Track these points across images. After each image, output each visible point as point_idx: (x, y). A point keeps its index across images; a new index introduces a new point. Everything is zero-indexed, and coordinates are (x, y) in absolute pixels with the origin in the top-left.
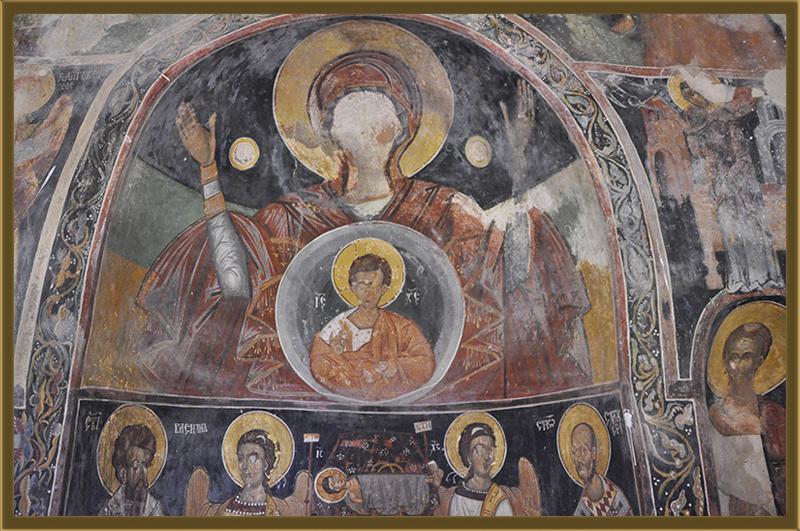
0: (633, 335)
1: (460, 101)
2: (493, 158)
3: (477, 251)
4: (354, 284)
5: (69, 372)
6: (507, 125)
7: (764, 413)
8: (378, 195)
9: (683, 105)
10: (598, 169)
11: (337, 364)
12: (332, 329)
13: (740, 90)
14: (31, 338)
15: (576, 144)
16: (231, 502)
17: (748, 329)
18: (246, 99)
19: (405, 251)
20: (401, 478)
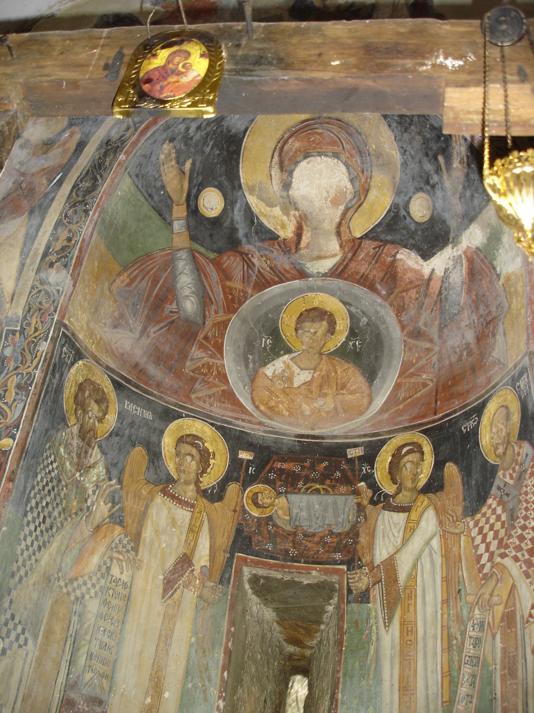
1: (405, 162)
2: (433, 211)
4: (300, 332)
5: (57, 307)
6: (445, 177)
11: (277, 397)
12: (276, 366)
16: (164, 488)
18: (218, 152)
19: (350, 305)
20: (329, 499)
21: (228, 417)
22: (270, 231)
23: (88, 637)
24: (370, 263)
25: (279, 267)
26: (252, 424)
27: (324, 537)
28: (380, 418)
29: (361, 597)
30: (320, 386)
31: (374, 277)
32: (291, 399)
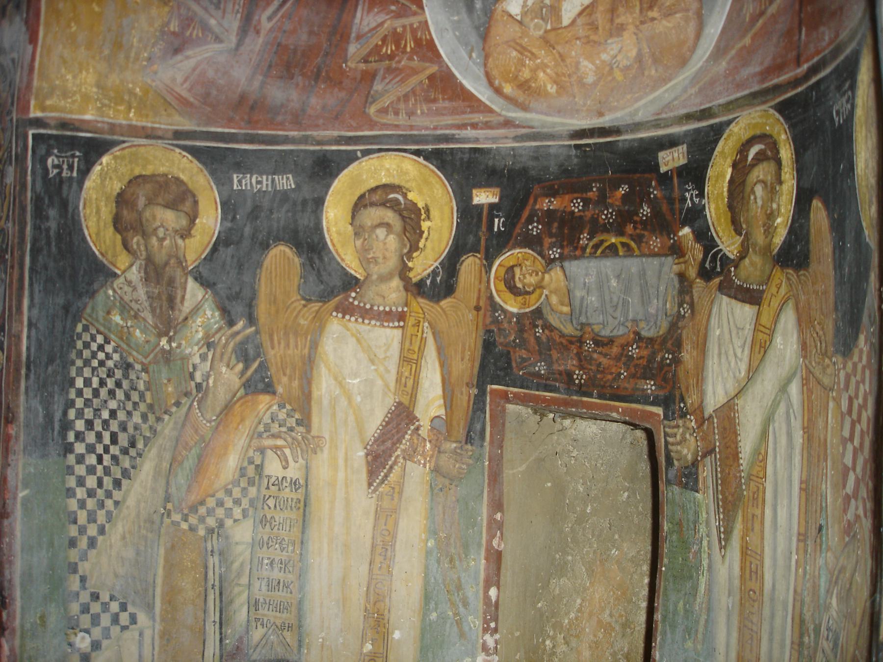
20: (633, 265)
21: (447, 127)
23: (244, 580)
26: (491, 128)
27: (628, 344)
29: (686, 476)
32: (561, 55)
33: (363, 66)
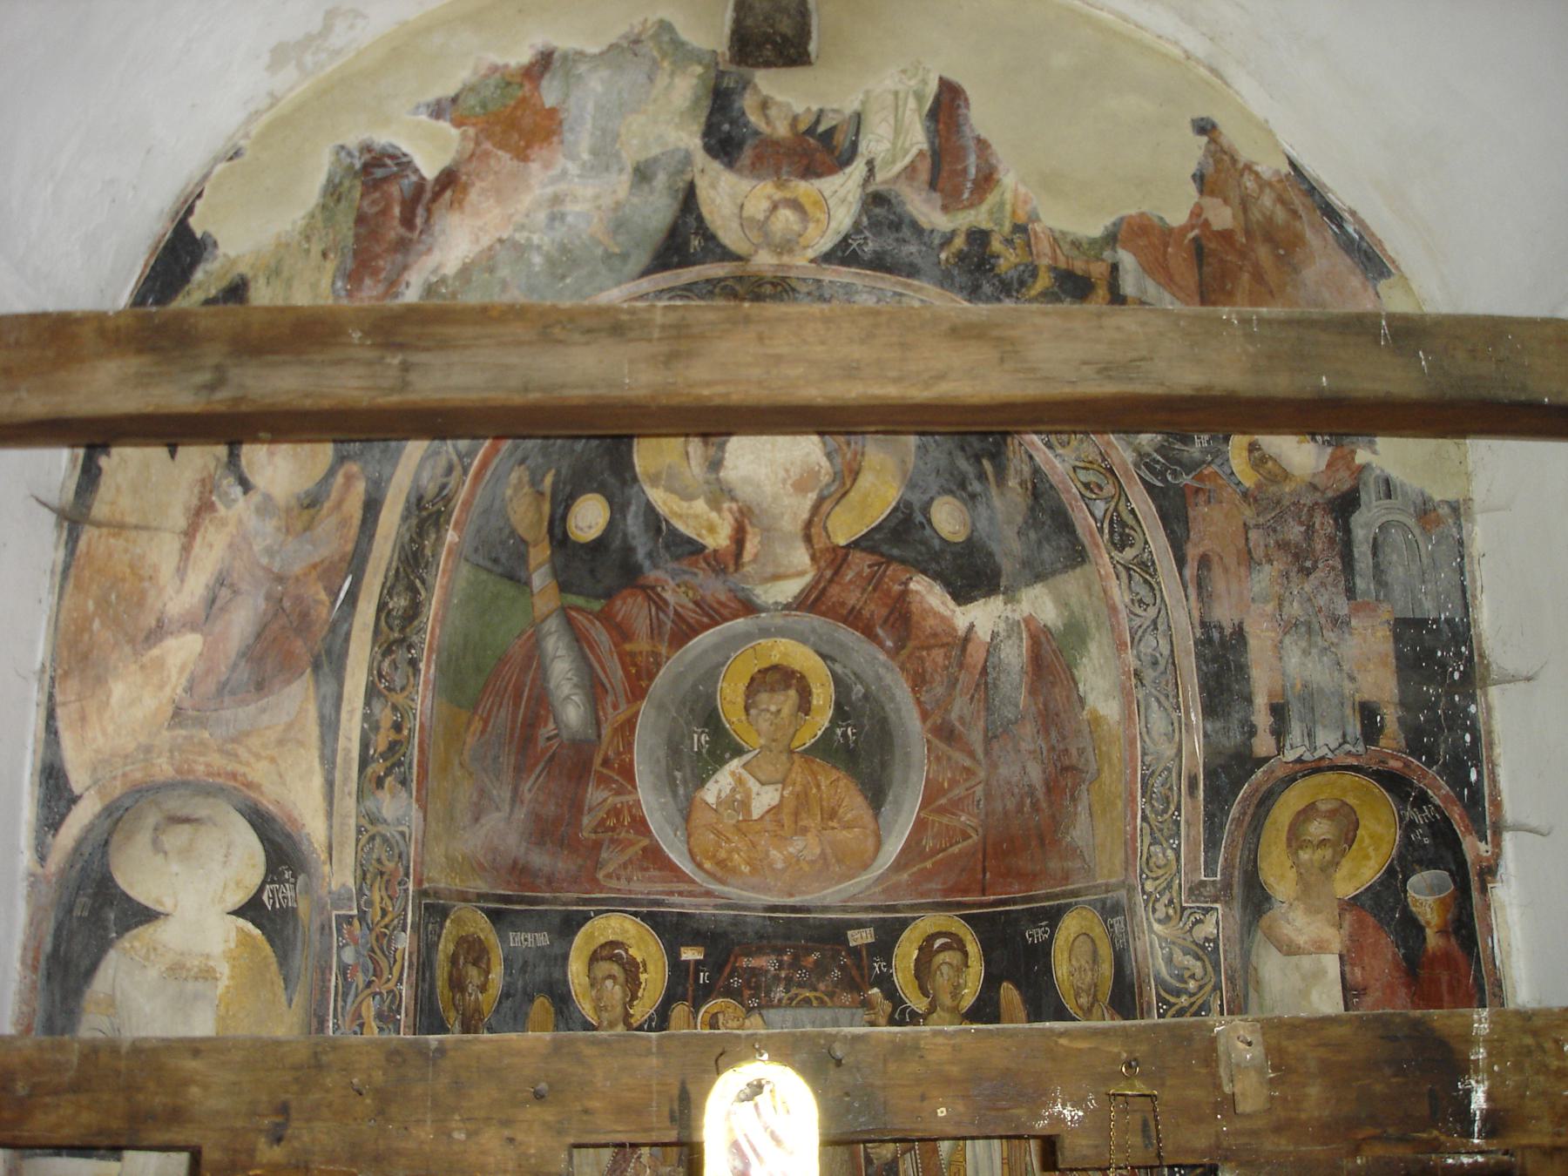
0: (1144, 818)
3: (946, 668)
4: (753, 712)
7: (1346, 925)
8: (792, 570)
9: (1248, 478)
10: (1115, 582)
11: (728, 840)
13: (1338, 453)
14: (352, 822)
15: (1086, 543)
17: (1323, 807)
19: (834, 660)
22: (690, 541)
24: (864, 590)
25: (709, 598)
28: (895, 879)
30: (794, 814)
31: (872, 614)
33: (593, 836)
